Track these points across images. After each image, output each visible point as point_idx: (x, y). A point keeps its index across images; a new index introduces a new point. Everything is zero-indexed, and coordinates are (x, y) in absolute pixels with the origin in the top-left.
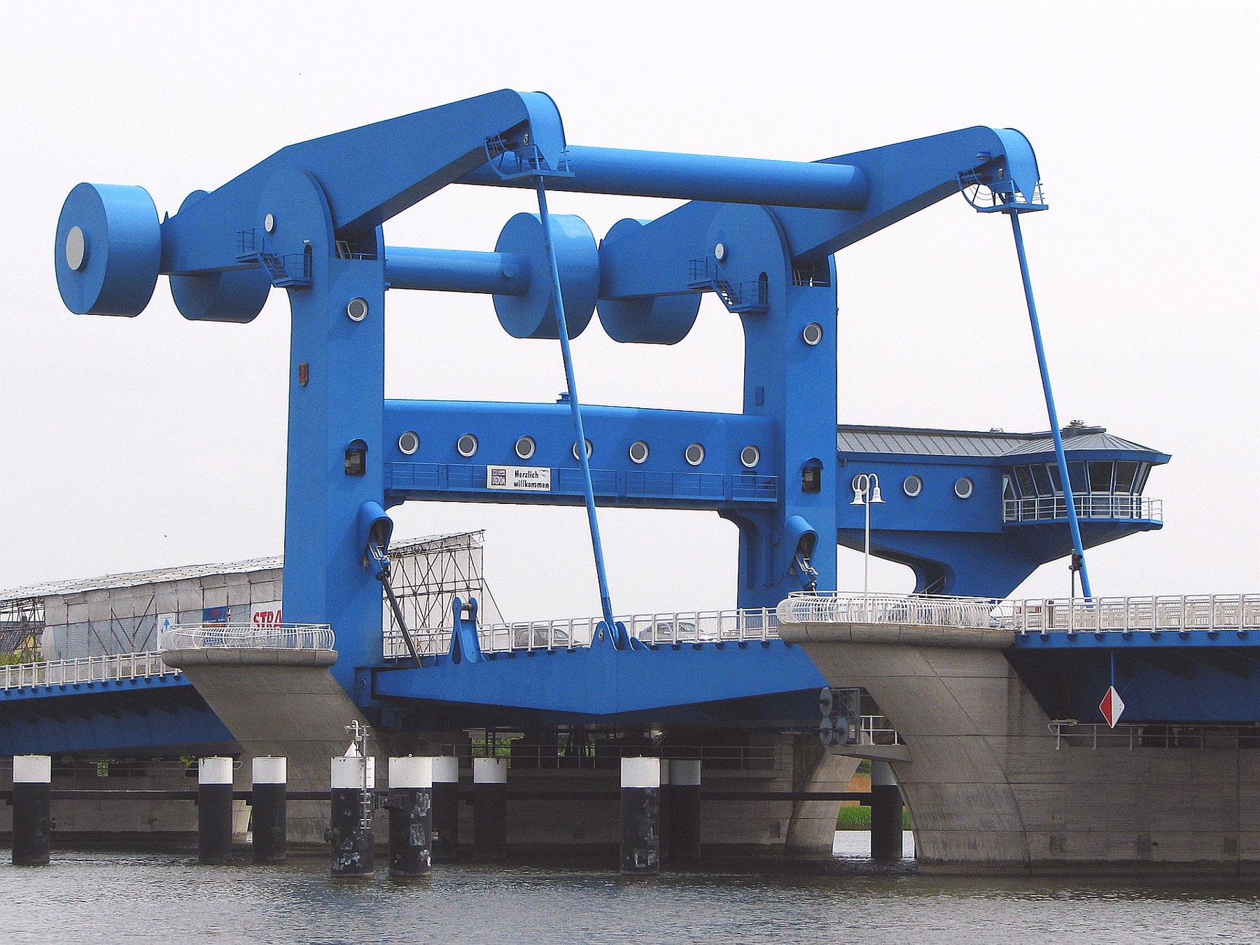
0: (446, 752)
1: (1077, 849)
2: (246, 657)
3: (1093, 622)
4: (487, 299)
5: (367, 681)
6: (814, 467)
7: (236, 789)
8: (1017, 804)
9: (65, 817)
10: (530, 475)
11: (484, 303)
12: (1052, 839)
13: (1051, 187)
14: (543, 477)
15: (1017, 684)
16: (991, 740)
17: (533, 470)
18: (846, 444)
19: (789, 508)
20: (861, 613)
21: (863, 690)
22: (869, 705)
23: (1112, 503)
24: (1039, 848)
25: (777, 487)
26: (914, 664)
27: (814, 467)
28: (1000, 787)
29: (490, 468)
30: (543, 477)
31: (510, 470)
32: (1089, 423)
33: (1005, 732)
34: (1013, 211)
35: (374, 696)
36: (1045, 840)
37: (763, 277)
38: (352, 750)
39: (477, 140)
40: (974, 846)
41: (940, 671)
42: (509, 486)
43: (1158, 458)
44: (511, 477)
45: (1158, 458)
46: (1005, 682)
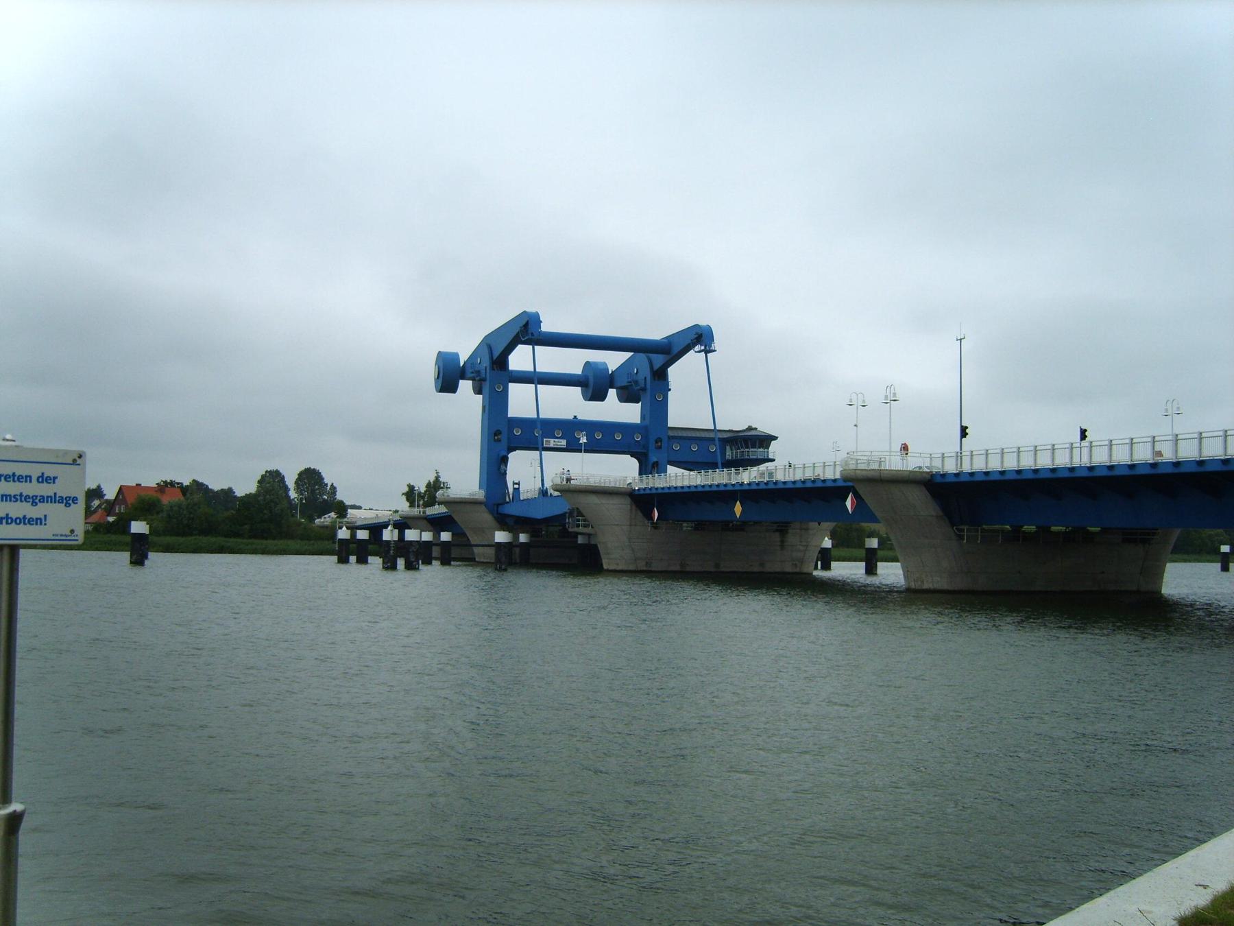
0: (527, 533)
1: (656, 566)
2: (456, 500)
3: (654, 484)
4: (579, 389)
5: (495, 509)
6: (659, 440)
7: (514, 544)
8: (633, 550)
9: (455, 552)
10: (558, 442)
11: (577, 390)
12: (647, 563)
13: (718, 343)
14: (563, 443)
15: (634, 507)
16: (623, 527)
17: (560, 440)
18: (671, 433)
19: (650, 454)
20: (616, 484)
21: (578, 509)
22: (580, 514)
23: (759, 453)
24: (641, 566)
25: (646, 447)
26: (593, 500)
27: (659, 440)
28: (627, 544)
29: (545, 439)
30: (563, 443)
31: (552, 440)
32: (753, 427)
33: (628, 523)
34: (707, 352)
35: (498, 513)
36: (644, 563)
37: (645, 378)
38: (389, 528)
39: (516, 330)
40: (618, 564)
41: (604, 502)
42: (552, 445)
43: (775, 438)
44: (553, 443)
45: (775, 438)
46: (629, 506)
